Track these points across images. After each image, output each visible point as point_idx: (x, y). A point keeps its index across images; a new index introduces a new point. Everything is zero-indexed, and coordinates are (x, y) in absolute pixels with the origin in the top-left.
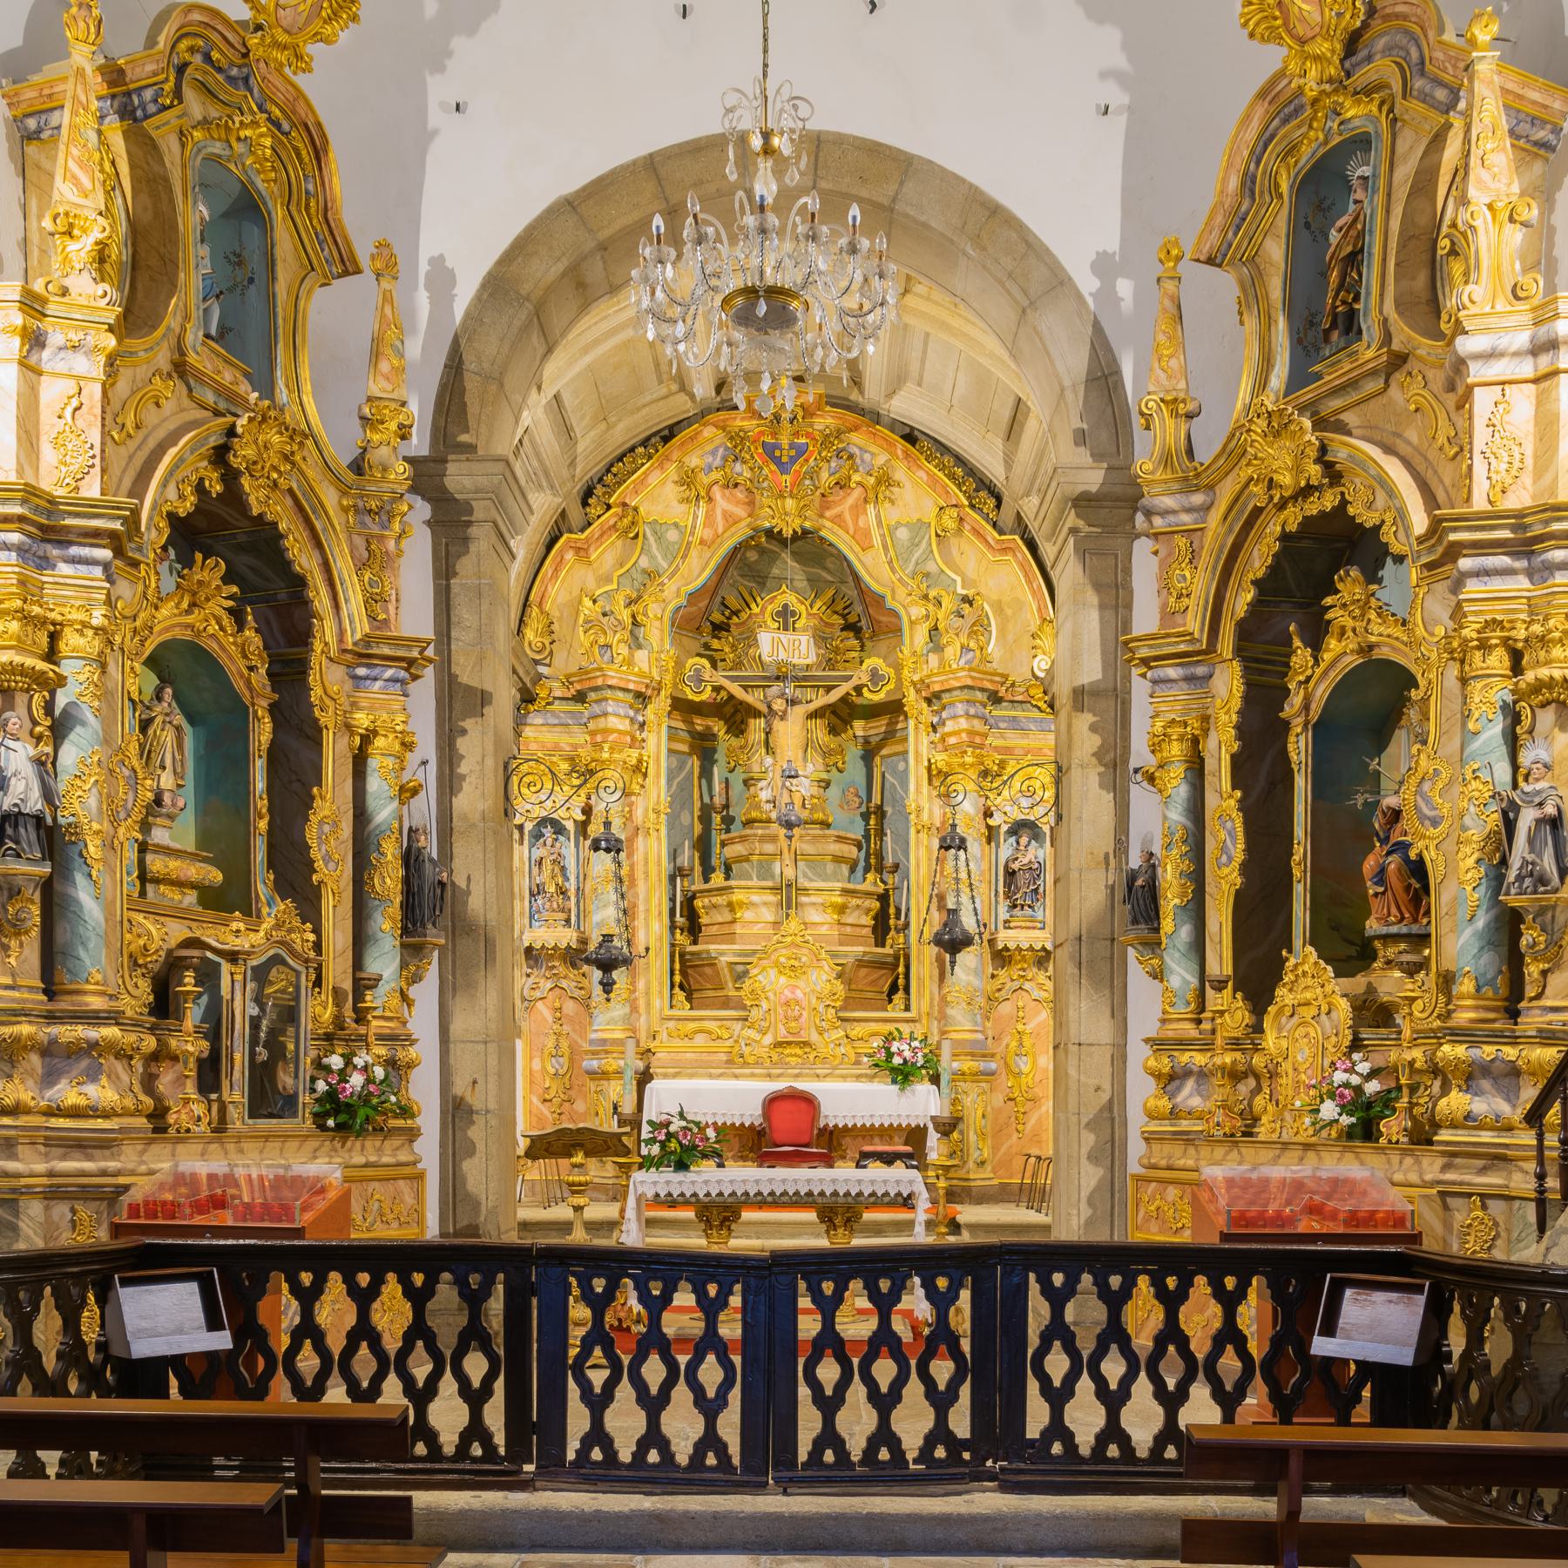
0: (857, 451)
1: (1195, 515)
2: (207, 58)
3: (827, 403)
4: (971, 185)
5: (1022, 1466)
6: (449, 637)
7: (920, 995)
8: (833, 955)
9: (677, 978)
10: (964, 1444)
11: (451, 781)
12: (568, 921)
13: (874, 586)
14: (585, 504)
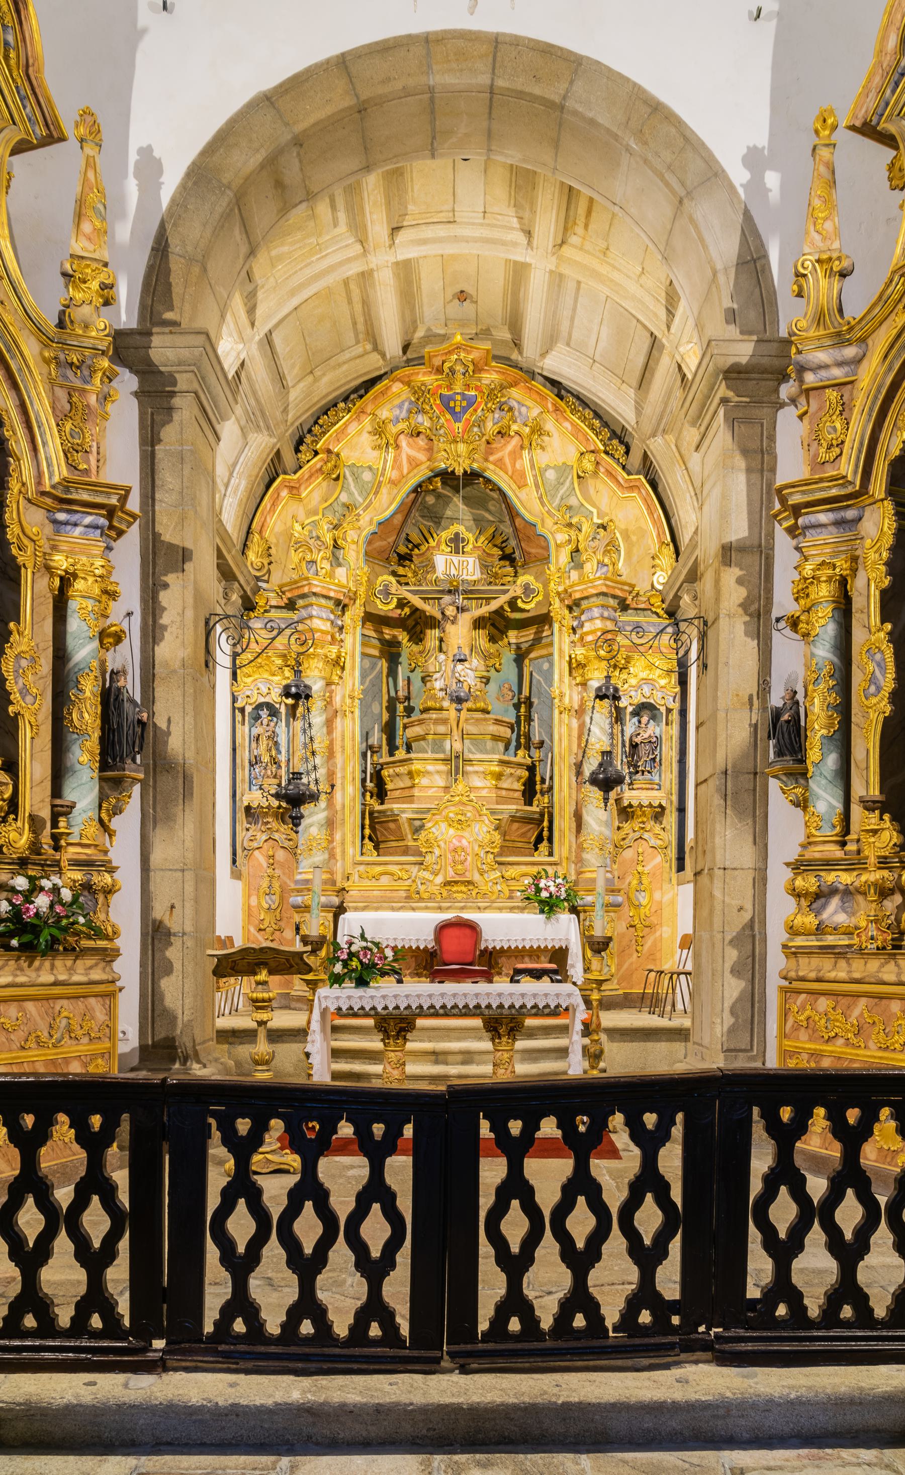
0: (515, 405)
1: (847, 369)
4: (635, 84)
5: (741, 1332)
6: (153, 499)
7: (561, 844)
8: (493, 812)
9: (367, 832)
10: (673, 1307)
11: (154, 631)
13: (527, 516)
14: (297, 450)
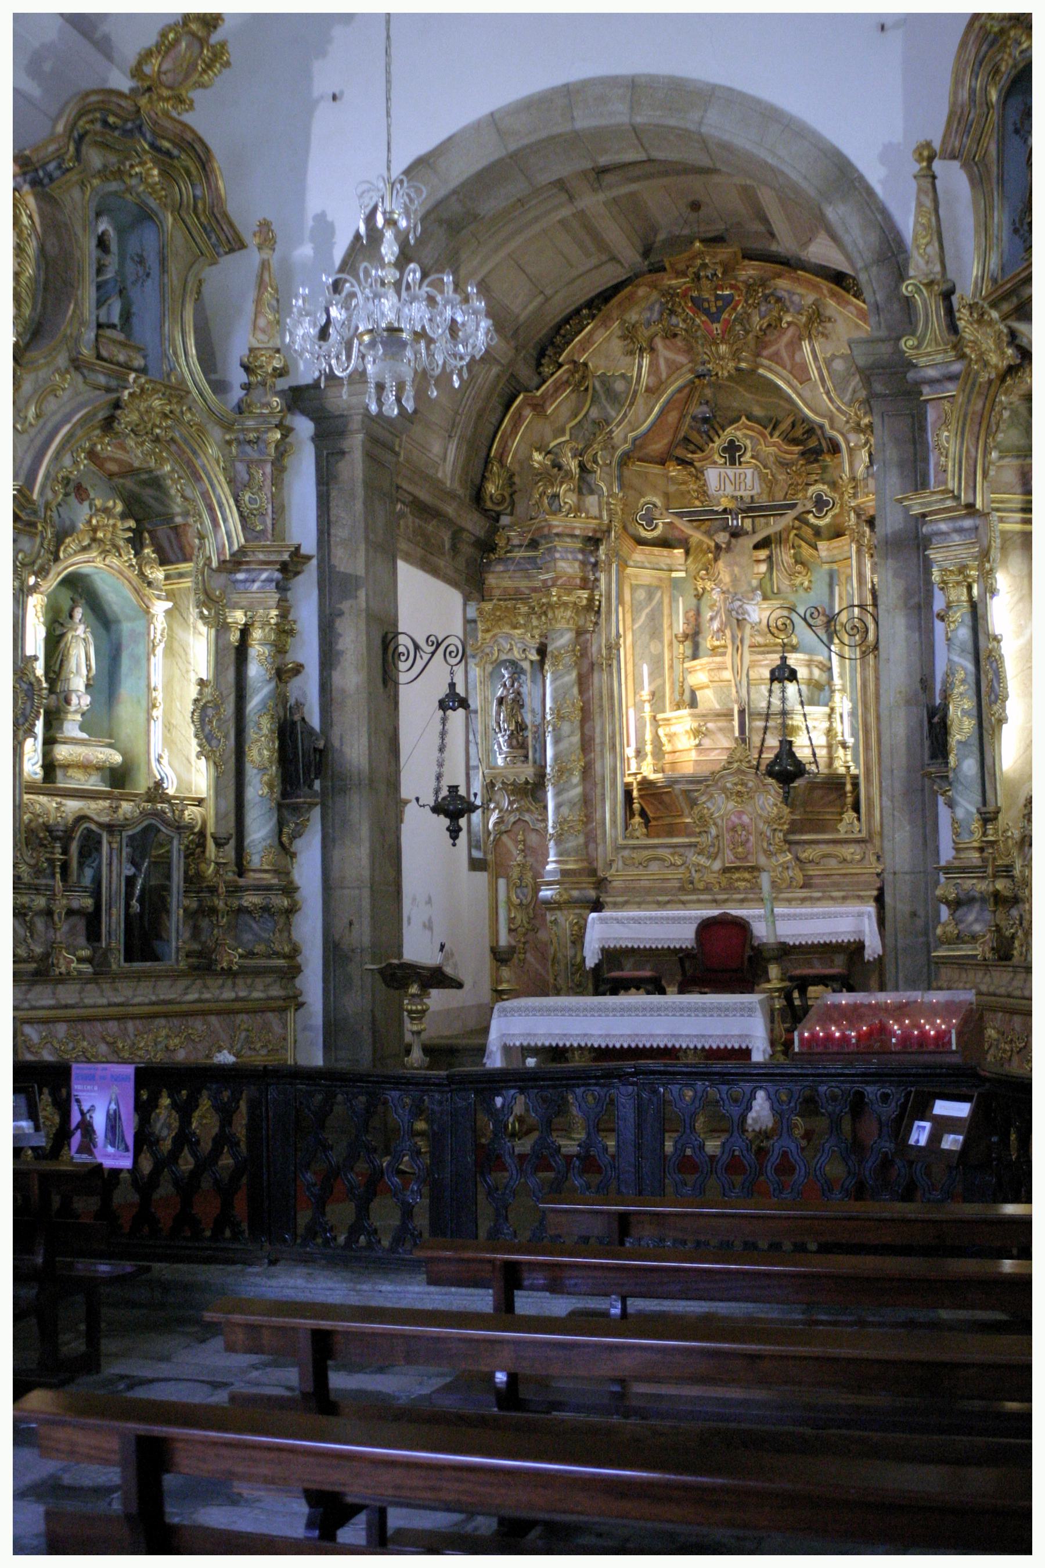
0: (785, 295)
2: (105, 123)
3: (744, 257)
12: (526, 757)
